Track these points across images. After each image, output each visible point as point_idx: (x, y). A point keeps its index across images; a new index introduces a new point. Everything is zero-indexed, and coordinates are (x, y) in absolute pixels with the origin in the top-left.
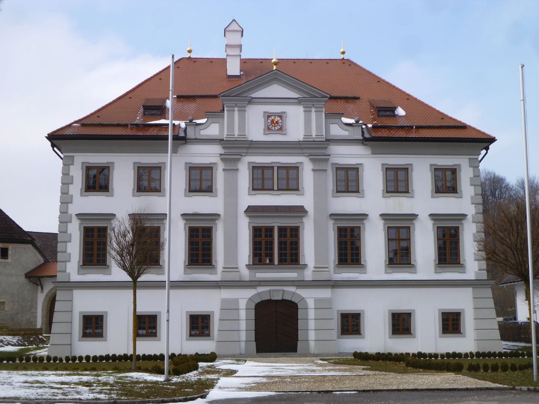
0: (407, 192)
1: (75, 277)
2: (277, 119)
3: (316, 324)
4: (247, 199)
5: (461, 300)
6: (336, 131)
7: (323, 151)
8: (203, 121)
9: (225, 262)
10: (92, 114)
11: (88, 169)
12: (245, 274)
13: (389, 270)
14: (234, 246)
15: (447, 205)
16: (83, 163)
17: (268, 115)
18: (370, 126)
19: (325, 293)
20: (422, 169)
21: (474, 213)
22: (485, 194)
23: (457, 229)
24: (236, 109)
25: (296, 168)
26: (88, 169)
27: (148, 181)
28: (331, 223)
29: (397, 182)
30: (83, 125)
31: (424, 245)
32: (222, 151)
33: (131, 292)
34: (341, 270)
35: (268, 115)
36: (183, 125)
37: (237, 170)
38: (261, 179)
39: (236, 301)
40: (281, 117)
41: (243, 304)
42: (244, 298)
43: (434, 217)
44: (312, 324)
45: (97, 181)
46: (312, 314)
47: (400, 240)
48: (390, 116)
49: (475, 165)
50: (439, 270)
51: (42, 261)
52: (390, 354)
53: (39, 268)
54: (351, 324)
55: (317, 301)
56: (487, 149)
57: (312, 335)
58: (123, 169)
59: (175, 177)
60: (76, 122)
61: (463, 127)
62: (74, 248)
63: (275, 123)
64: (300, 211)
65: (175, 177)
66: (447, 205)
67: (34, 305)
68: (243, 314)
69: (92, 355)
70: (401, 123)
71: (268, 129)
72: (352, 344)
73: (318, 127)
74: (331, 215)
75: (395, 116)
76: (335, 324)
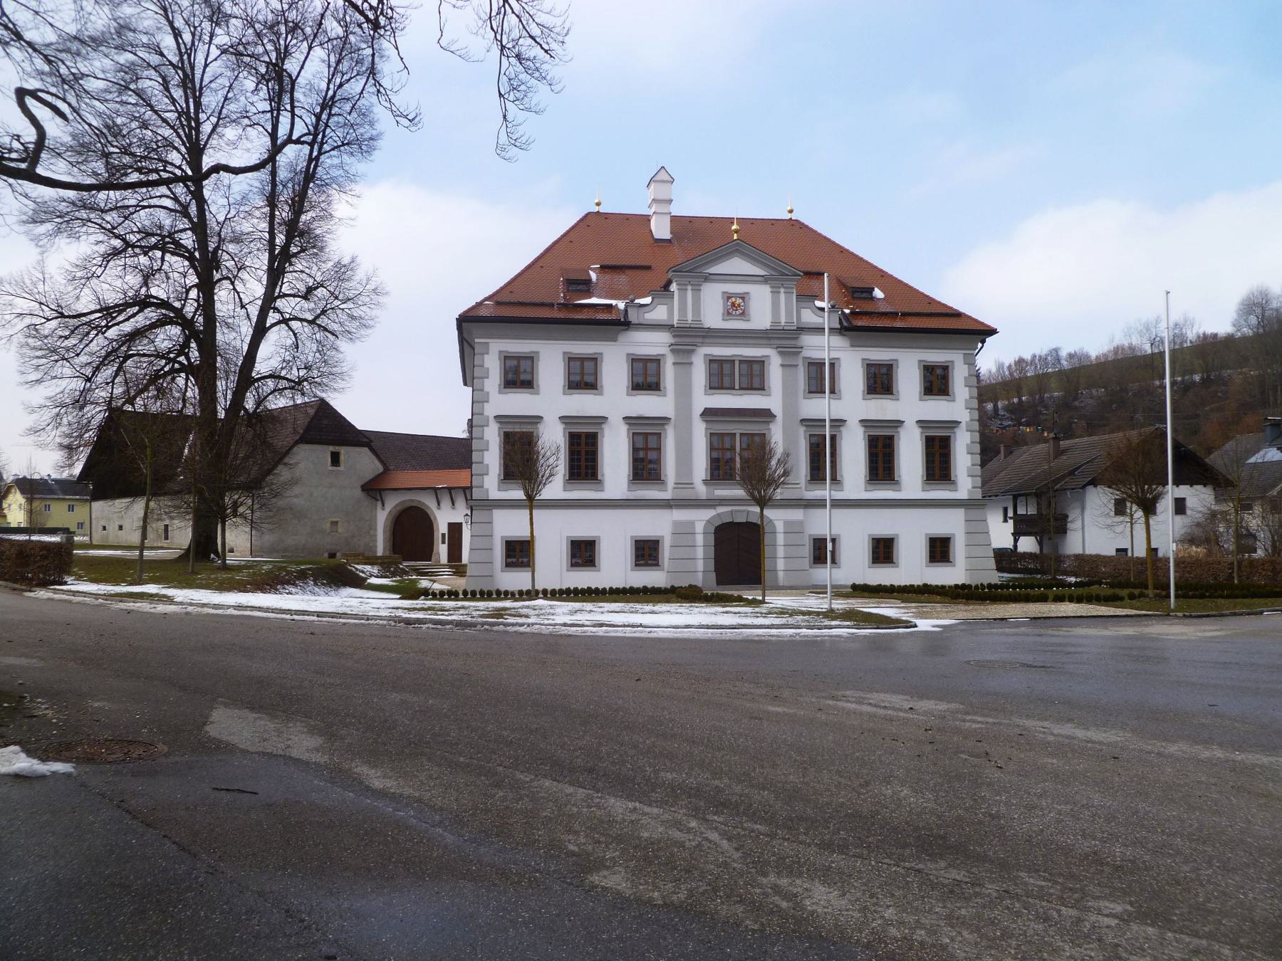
0: (763, 389)
1: (495, 494)
2: (739, 301)
3: (785, 551)
4: (703, 399)
5: (951, 523)
6: (809, 317)
7: (793, 342)
8: (647, 300)
9: (678, 474)
10: (502, 289)
11: (506, 358)
12: (702, 491)
13: (870, 487)
14: (687, 457)
15: (937, 409)
16: (500, 352)
17: (727, 296)
18: (847, 311)
19: (796, 515)
20: (909, 366)
21: (968, 419)
22: (1042, 399)
23: (891, 438)
24: (689, 287)
25: (761, 363)
26: (506, 358)
27: (583, 377)
28: (802, 430)
29: (880, 381)
30: (498, 303)
31: (910, 456)
32: (672, 341)
33: (527, 512)
34: (814, 486)
35: (727, 296)
36: (621, 305)
37: (691, 363)
38: (721, 376)
39: (692, 523)
40: (743, 298)
41: (699, 527)
42: (701, 519)
43: (922, 424)
44: (781, 552)
45: (519, 376)
46: (780, 539)
47: (724, 449)
48: (865, 298)
49: (970, 361)
50: (927, 487)
51: (381, 469)
52: (912, 586)
53: (378, 478)
54: (822, 551)
55: (787, 523)
56: (983, 342)
57: (781, 564)
58: (551, 359)
59: (614, 372)
60: (486, 299)
61: (957, 315)
62: (491, 458)
63: (736, 306)
64: (766, 415)
65: (614, 372)
66: (937, 409)
67: (373, 527)
68: (700, 539)
69: (549, 588)
70: (884, 308)
71: (728, 314)
72: (824, 574)
73: (789, 312)
74: (803, 420)
75: (872, 298)
76: (807, 551)
